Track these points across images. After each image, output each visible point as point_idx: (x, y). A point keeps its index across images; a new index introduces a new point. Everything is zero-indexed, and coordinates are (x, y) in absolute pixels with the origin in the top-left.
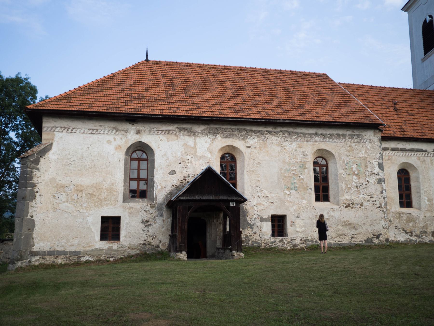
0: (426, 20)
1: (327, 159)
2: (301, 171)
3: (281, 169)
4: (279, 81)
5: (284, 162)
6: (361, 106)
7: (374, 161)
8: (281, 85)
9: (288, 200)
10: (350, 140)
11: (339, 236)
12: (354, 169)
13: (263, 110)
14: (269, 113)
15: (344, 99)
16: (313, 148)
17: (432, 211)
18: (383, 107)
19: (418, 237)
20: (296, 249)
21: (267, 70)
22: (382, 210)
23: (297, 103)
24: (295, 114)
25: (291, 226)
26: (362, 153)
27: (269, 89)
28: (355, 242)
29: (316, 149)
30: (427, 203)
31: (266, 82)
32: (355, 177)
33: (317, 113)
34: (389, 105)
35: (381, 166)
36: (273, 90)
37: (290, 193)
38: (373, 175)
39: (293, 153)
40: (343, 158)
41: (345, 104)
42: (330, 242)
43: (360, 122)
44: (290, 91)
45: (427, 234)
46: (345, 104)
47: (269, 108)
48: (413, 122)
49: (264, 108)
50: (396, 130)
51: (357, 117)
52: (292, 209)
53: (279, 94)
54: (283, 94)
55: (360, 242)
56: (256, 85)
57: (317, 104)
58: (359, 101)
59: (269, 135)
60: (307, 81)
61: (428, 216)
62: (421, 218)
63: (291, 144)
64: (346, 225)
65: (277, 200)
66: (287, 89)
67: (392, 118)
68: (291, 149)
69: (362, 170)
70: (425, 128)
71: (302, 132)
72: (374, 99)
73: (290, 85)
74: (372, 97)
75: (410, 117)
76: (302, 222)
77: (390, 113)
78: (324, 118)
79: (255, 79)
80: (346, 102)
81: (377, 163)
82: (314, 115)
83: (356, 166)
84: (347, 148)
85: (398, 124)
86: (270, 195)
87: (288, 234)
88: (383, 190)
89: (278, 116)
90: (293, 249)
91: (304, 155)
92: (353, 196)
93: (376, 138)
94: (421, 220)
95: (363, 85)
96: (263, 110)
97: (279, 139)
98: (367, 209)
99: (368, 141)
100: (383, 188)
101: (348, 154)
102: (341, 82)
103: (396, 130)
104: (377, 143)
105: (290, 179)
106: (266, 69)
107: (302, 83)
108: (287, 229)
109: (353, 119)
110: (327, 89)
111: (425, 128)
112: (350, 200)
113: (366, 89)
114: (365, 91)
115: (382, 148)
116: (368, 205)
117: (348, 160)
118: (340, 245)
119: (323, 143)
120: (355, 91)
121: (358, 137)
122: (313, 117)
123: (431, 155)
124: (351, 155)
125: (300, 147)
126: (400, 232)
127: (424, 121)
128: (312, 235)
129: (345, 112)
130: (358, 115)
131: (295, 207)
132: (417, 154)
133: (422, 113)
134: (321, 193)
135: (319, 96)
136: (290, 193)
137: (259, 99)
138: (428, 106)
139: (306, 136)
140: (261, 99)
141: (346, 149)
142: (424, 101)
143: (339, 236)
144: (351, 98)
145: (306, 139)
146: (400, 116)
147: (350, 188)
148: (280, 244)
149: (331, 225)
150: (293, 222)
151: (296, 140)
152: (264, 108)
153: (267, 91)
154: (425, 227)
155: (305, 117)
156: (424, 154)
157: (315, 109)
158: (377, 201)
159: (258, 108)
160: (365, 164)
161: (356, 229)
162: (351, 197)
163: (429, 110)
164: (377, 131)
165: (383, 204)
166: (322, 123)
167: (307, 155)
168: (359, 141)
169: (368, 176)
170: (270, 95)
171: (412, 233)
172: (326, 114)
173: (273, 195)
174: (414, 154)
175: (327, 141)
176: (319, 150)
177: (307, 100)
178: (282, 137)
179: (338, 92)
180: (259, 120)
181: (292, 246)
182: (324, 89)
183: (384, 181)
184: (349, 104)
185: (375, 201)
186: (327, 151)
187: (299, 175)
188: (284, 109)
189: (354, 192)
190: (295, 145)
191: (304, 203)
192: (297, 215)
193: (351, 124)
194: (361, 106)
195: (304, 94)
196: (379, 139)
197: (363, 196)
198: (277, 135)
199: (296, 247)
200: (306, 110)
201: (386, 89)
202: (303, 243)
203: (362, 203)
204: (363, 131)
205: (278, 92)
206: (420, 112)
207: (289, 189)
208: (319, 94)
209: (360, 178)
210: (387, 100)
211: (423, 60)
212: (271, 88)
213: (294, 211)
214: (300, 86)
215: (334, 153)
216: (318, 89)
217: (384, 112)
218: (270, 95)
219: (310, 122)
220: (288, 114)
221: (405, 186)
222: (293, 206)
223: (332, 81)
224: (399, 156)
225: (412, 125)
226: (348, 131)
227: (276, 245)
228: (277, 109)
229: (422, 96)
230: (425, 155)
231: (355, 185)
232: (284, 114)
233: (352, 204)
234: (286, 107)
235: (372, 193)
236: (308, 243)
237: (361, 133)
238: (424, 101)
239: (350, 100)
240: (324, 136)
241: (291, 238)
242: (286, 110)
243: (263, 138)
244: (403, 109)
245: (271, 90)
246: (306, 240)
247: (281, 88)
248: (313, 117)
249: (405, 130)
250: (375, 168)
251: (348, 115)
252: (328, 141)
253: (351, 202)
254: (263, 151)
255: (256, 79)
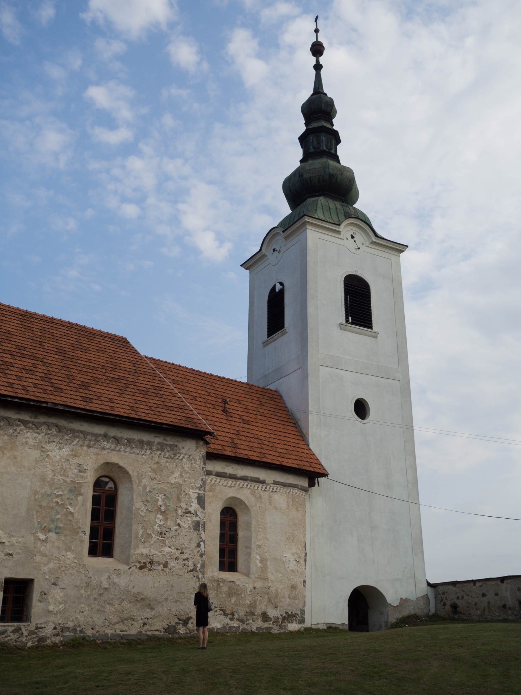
0: (274, 286)
1: (117, 481)
2: (72, 499)
3: (36, 492)
4: (48, 336)
5: (43, 479)
6: (178, 399)
7: (191, 491)
8: (51, 343)
9: (40, 551)
10: (159, 452)
11: (123, 620)
12: (160, 503)
13: (18, 382)
14: (29, 388)
15: (153, 384)
16: (97, 459)
17: (265, 579)
18: (208, 405)
19: (241, 621)
20: (43, 647)
21: (29, 313)
22: (196, 575)
23: (77, 378)
24: (75, 397)
25: (40, 601)
26: (175, 476)
27: (30, 347)
28: (148, 633)
29: (102, 462)
30: (259, 565)
31: (27, 333)
32: (159, 516)
33: (111, 400)
34: (217, 403)
35: (201, 501)
36: (37, 348)
37: (47, 538)
38: (188, 515)
39: (62, 465)
40: (144, 481)
41: (155, 391)
42: (106, 631)
43: (177, 424)
44: (67, 356)
45: (254, 617)
46: (155, 391)
47: (30, 380)
48: (248, 435)
49: (19, 378)
50: (225, 444)
51: (174, 417)
52: (45, 569)
53: (48, 358)
54: (53, 359)
55: (157, 633)
56: (8, 335)
57: (111, 386)
58: (177, 391)
59: (22, 427)
60: (95, 345)
61: (259, 586)
62: (249, 590)
63: (60, 449)
64: (137, 600)
65: (19, 551)
66: (61, 352)
67: (221, 425)
68: (58, 458)
69: (172, 504)
70: (264, 447)
71: (81, 429)
72: (194, 390)
73: (67, 347)
74: (192, 386)
75: (245, 426)
76: (61, 594)
77: (217, 416)
78: (122, 410)
79: (7, 326)
80: (157, 388)
81: (197, 495)
82: (106, 403)
83: (163, 497)
84: (152, 465)
85: (227, 435)
86: (9, 540)
87: (32, 618)
88: (201, 541)
89: (45, 396)
90: (37, 647)
91: (80, 471)
92: (154, 549)
93: (199, 454)
94: (249, 593)
95: (179, 366)
96: (18, 382)
97: (40, 437)
98: (173, 573)
99: (186, 457)
100: (201, 538)
101: (153, 475)
102: (147, 356)
103: (226, 445)
104: (199, 462)
105: (49, 513)
106: (27, 312)
107: (88, 346)
108: (31, 606)
109: (167, 419)
110: (127, 363)
111: (264, 447)
112: (147, 556)
113: (185, 373)
114: (183, 376)
115: (207, 471)
116: (175, 567)
117: (152, 486)
118: (122, 637)
119: (114, 452)
120: (168, 372)
121: (172, 450)
122: (103, 407)
123: (270, 488)
124: (158, 478)
125: (75, 456)
126: (216, 614)
127: (264, 434)
128: (76, 618)
129: (155, 406)
130: (174, 413)
131: (51, 565)
132: (251, 486)
133: (261, 422)
134: (100, 541)
135: (114, 373)
136: (47, 538)
137: (12, 361)
138: (270, 412)
139: (88, 437)
140: (15, 361)
141: (150, 467)
142: (264, 404)
143: (123, 620)
144: (164, 383)
145: (87, 443)
146: (230, 423)
147: (150, 535)
148: (14, 637)
149: (112, 600)
150: (45, 594)
151: (69, 441)
152: (19, 378)
153: (28, 350)
154: (253, 605)
155: (91, 404)
156: (260, 486)
157: (107, 392)
158: (190, 560)
159: (9, 376)
160: (178, 495)
161: (152, 609)
162: (150, 551)
163: (270, 419)
164: (202, 443)
165: (199, 566)
166: (118, 418)
167: (85, 471)
168: (172, 456)
169: (181, 516)
170: (32, 358)
171: (233, 615)
172: (125, 403)
173: (14, 540)
174: (247, 485)
175: (122, 450)
176: (107, 463)
177: (94, 375)
178: (46, 434)
179: (144, 370)
180: (9, 399)
181: (35, 639)
182: (122, 362)
183: (204, 527)
184: (161, 392)
185: (187, 559)
186: (120, 467)
187: (66, 506)
188: (56, 385)
189: (155, 542)
190: (66, 451)
191: (69, 559)
192: (53, 581)
193: (164, 426)
194: (178, 399)
195: (90, 364)
196: (203, 457)
197: (170, 550)
198: (38, 429)
199: (44, 642)
200: (92, 393)
201: (213, 378)
202: (57, 635)
203: (167, 562)
204: (180, 440)
205: (45, 354)
206: (258, 421)
207: (46, 530)
208: (114, 369)
209: (167, 518)
210: (214, 395)
211: (265, 344)
212: (34, 345)
213: (50, 572)
214: (83, 351)
215: (131, 473)
216: (112, 360)
217: (209, 414)
218: (32, 358)
219: (99, 415)
220: (62, 394)
221: (230, 535)
222: (49, 562)
223: (135, 352)
224: (226, 486)
225: (248, 439)
226: (156, 437)
227: (6, 639)
228: (42, 383)
229: (261, 396)
230: (262, 487)
231: (159, 530)
232: (55, 393)
233: (150, 562)
234: (59, 382)
235: (183, 546)
236: (67, 634)
237: (176, 443)
238: (264, 404)
239: (163, 386)
240: (117, 440)
241: (36, 624)
242: (58, 388)
243: (11, 431)
244: (235, 412)
245: (33, 348)
246: (64, 629)
247: (51, 349)
248: (103, 407)
249: (238, 445)
250: (192, 504)
251: (159, 410)
252: (124, 451)
253: (149, 560)
254: (8, 455)
255: (9, 326)
